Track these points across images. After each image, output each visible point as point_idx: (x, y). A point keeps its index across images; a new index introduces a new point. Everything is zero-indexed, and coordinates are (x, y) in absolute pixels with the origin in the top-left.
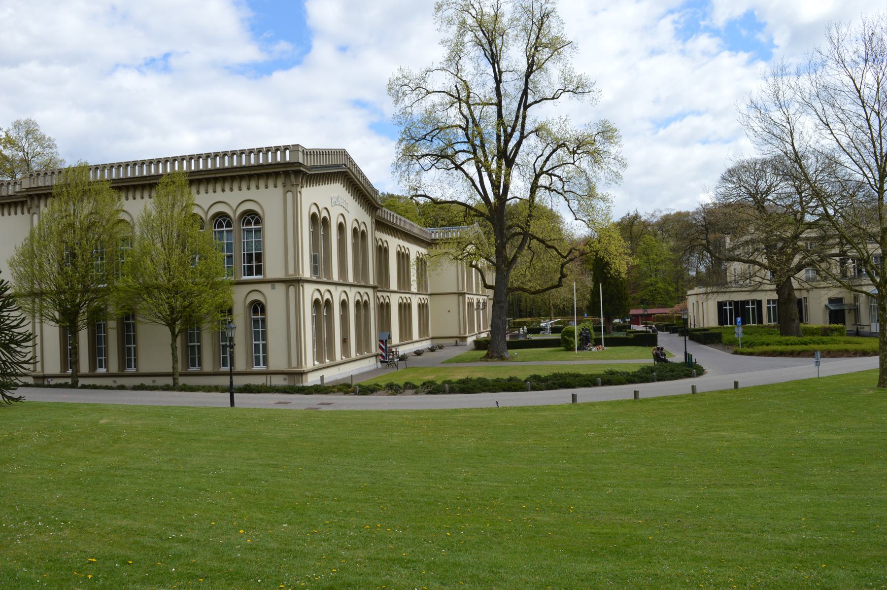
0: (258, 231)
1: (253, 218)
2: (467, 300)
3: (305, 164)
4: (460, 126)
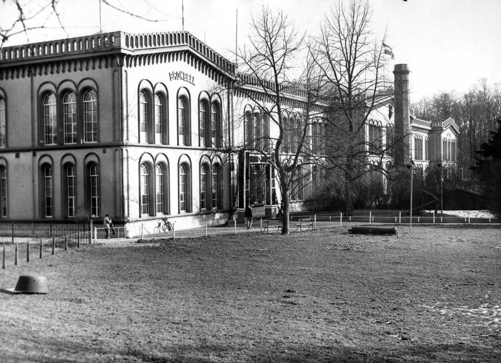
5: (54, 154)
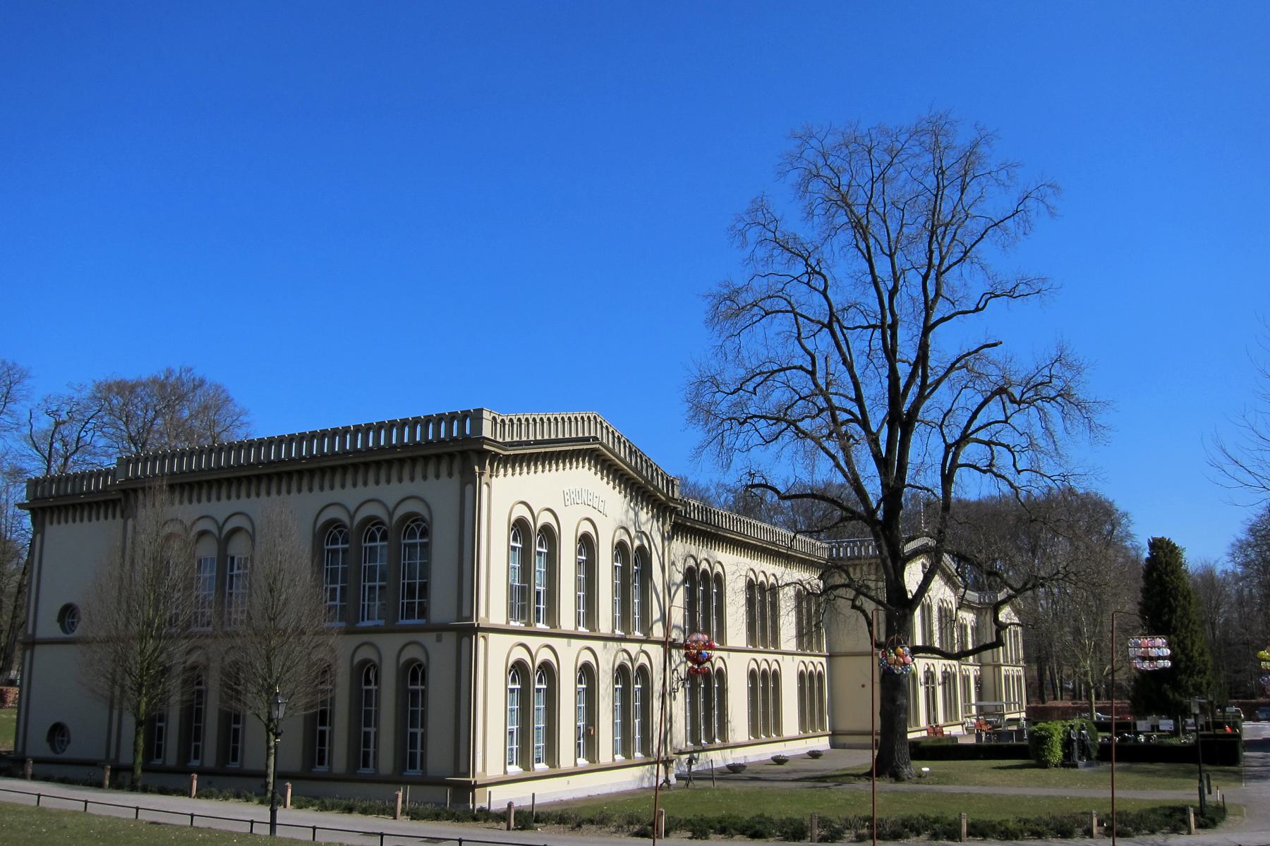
0: (425, 546)
1: (418, 526)
2: (1003, 673)
3: (499, 439)
4: (801, 368)
5: (379, 640)
